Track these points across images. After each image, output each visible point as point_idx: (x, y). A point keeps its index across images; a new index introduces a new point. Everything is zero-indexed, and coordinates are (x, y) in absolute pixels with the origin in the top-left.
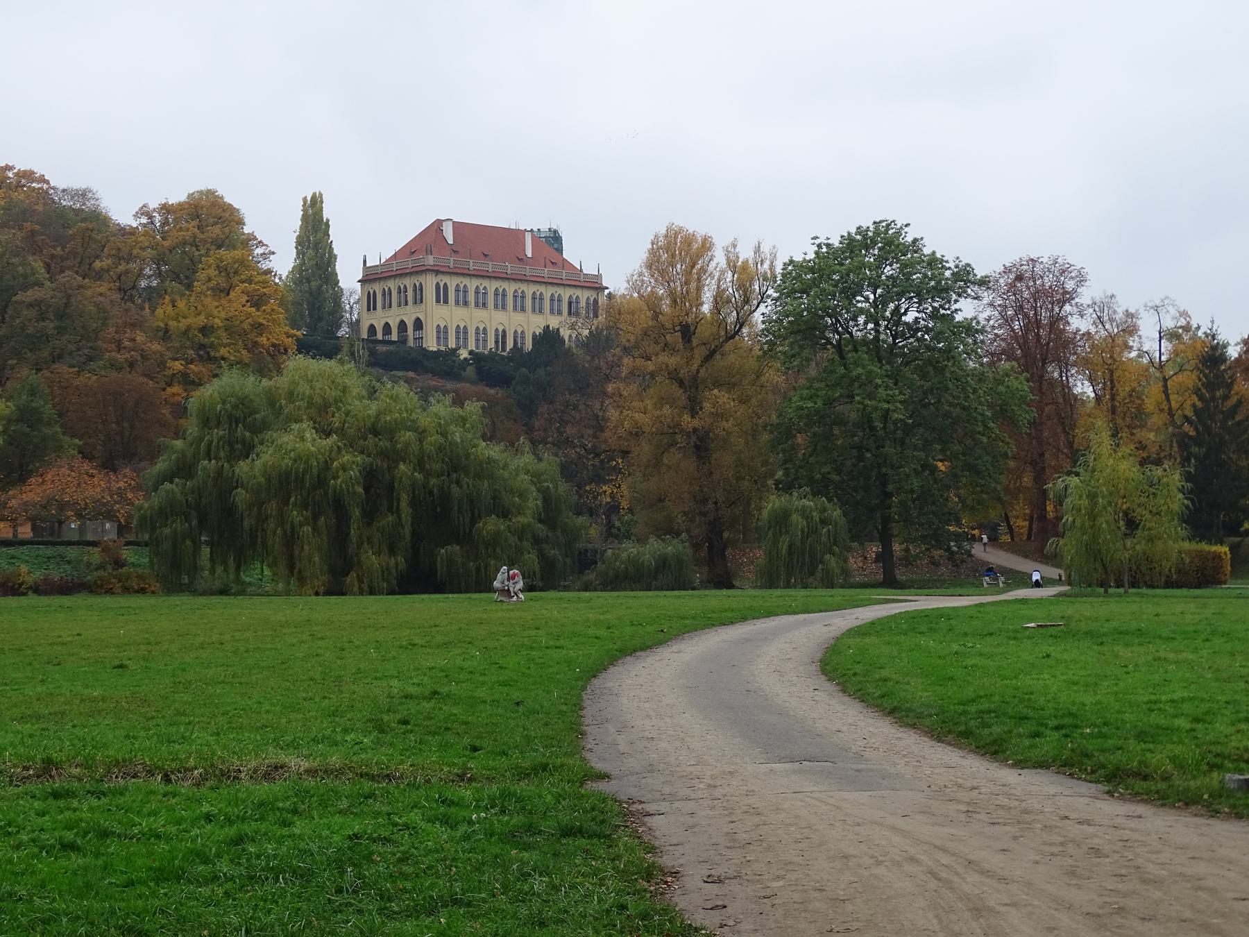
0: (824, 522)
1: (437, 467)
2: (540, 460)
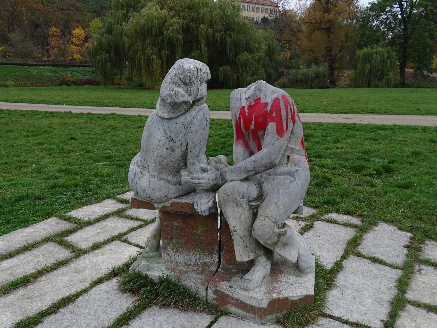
0: (389, 58)
1: (219, 27)
2: (267, 31)
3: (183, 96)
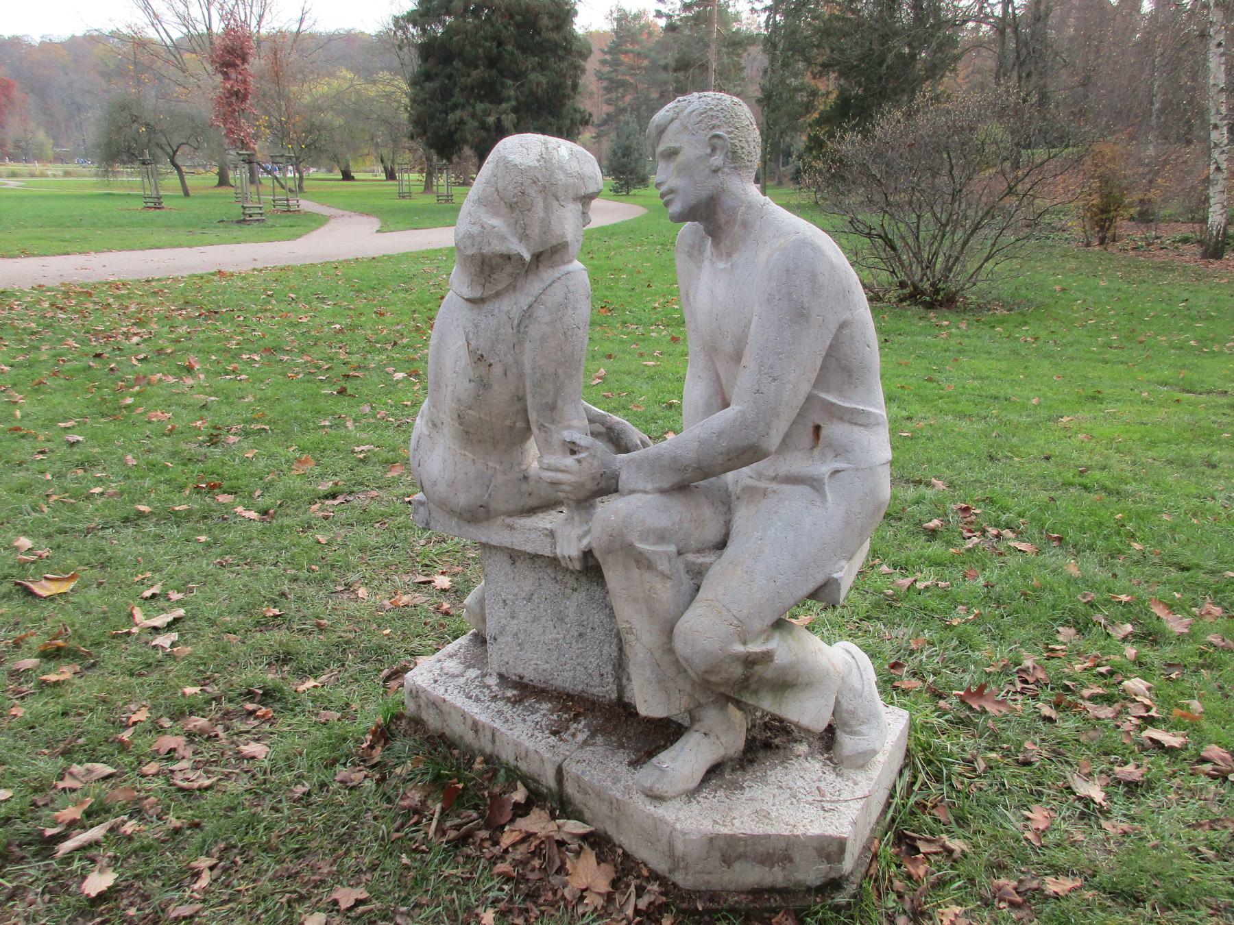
3: (503, 238)
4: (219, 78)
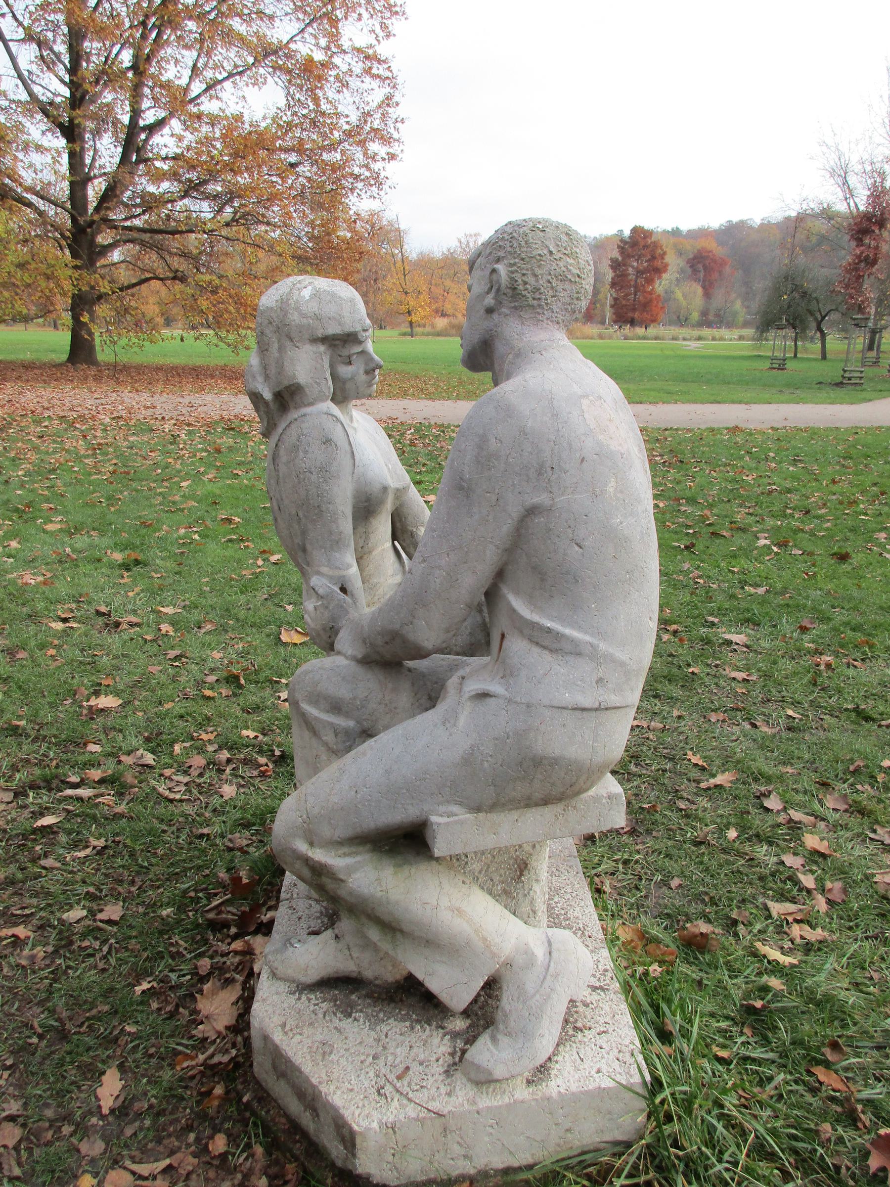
4: (853, 244)
